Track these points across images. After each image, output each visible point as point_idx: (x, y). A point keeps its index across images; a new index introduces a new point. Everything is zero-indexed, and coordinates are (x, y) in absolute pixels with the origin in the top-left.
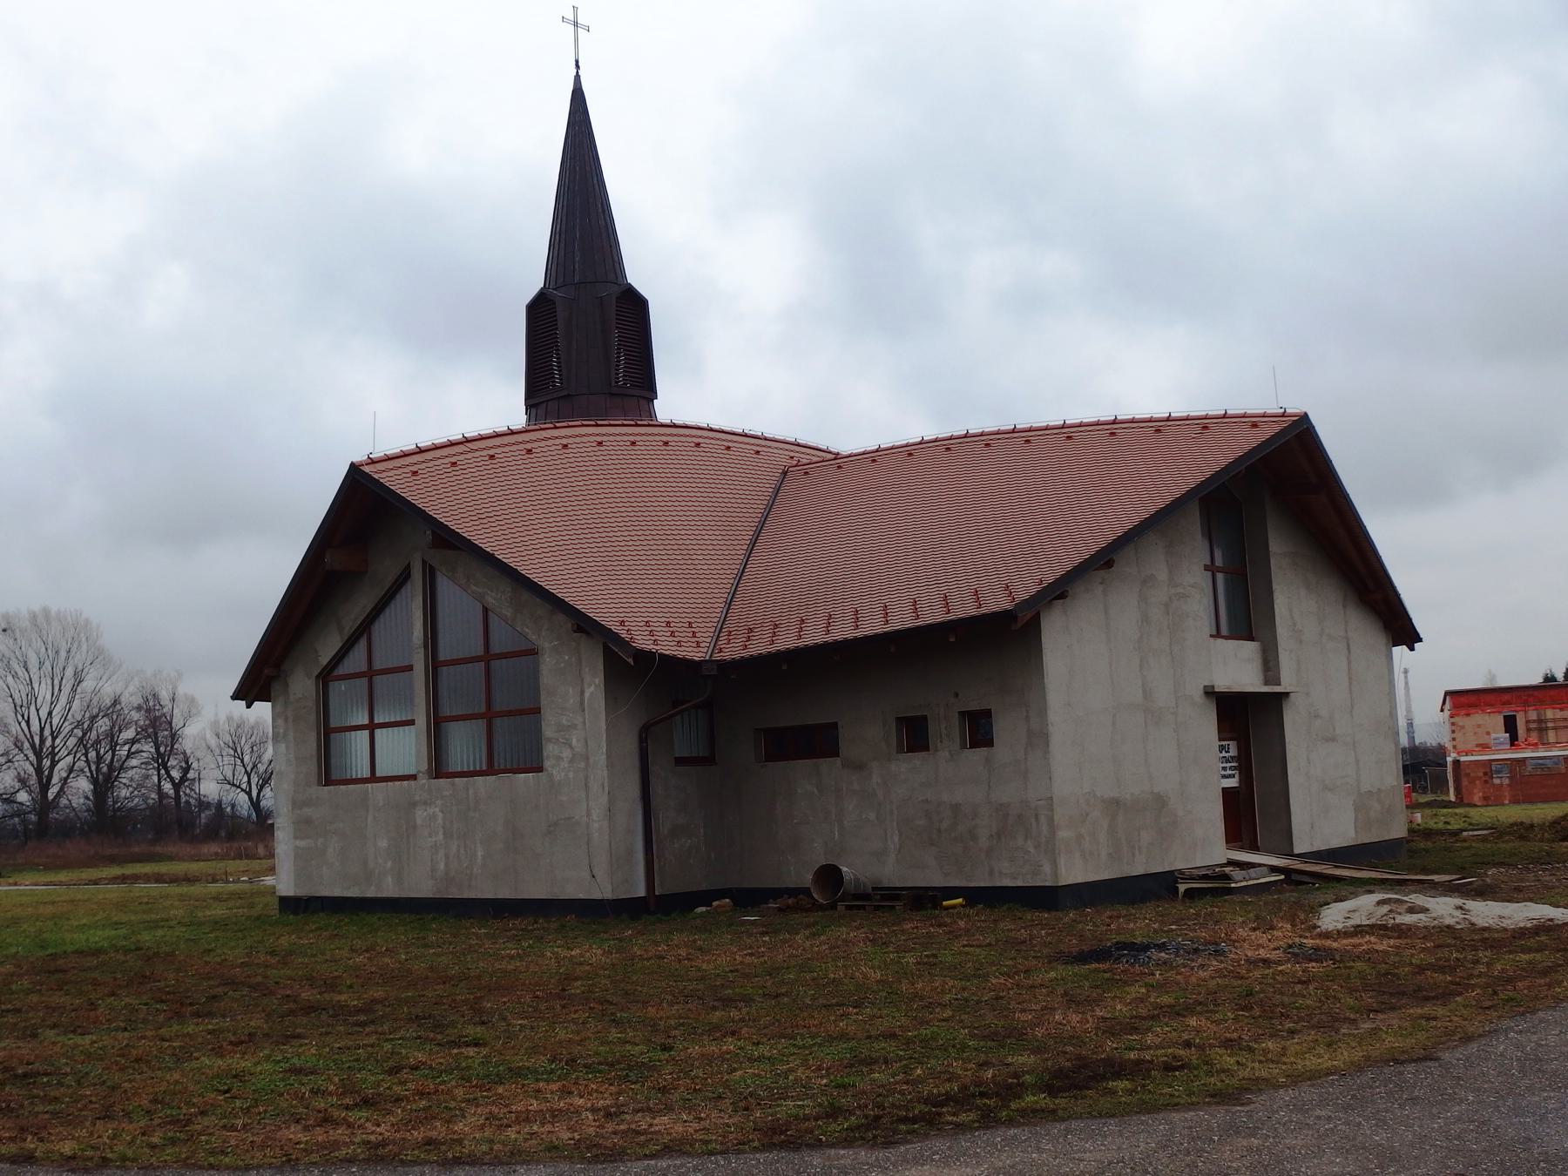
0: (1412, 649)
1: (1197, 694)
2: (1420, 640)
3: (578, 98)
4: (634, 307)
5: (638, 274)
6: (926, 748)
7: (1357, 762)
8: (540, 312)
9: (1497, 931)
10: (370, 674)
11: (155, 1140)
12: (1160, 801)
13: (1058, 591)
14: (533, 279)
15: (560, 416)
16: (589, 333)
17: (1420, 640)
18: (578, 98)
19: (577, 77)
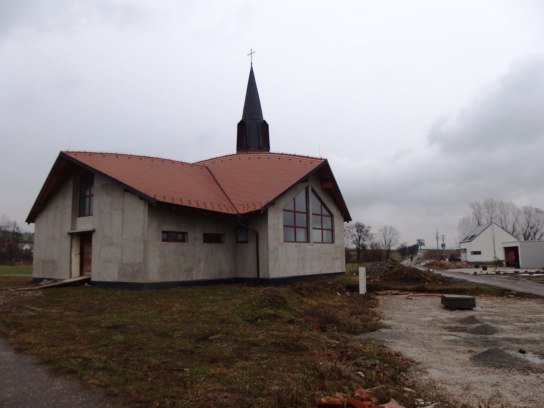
0: (29, 224)
1: (66, 235)
2: (351, 220)
3: (252, 73)
4: (265, 126)
5: (266, 117)
6: (221, 242)
7: (122, 252)
8: (241, 125)
9: (410, 291)
10: (322, 215)
11: (119, 337)
12: (54, 261)
13: (272, 203)
14: (239, 118)
15: (241, 152)
16: (253, 131)
17: (351, 220)
18: (252, 73)
19: (252, 67)
